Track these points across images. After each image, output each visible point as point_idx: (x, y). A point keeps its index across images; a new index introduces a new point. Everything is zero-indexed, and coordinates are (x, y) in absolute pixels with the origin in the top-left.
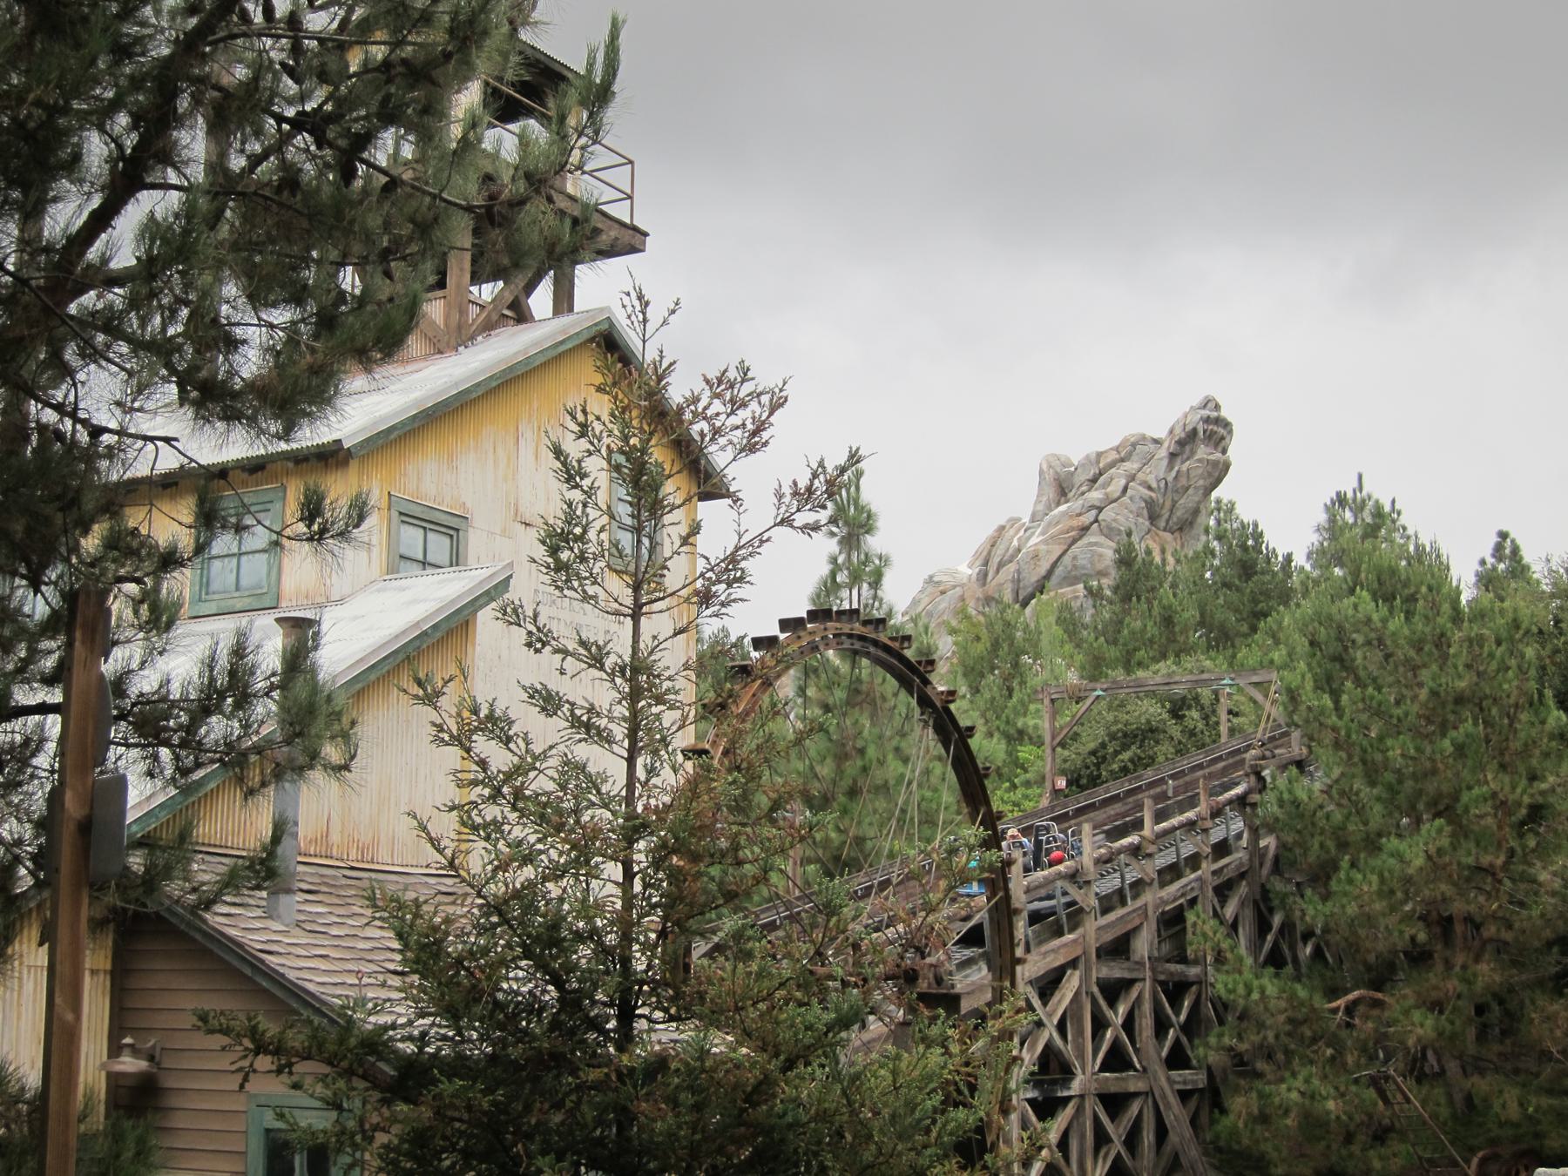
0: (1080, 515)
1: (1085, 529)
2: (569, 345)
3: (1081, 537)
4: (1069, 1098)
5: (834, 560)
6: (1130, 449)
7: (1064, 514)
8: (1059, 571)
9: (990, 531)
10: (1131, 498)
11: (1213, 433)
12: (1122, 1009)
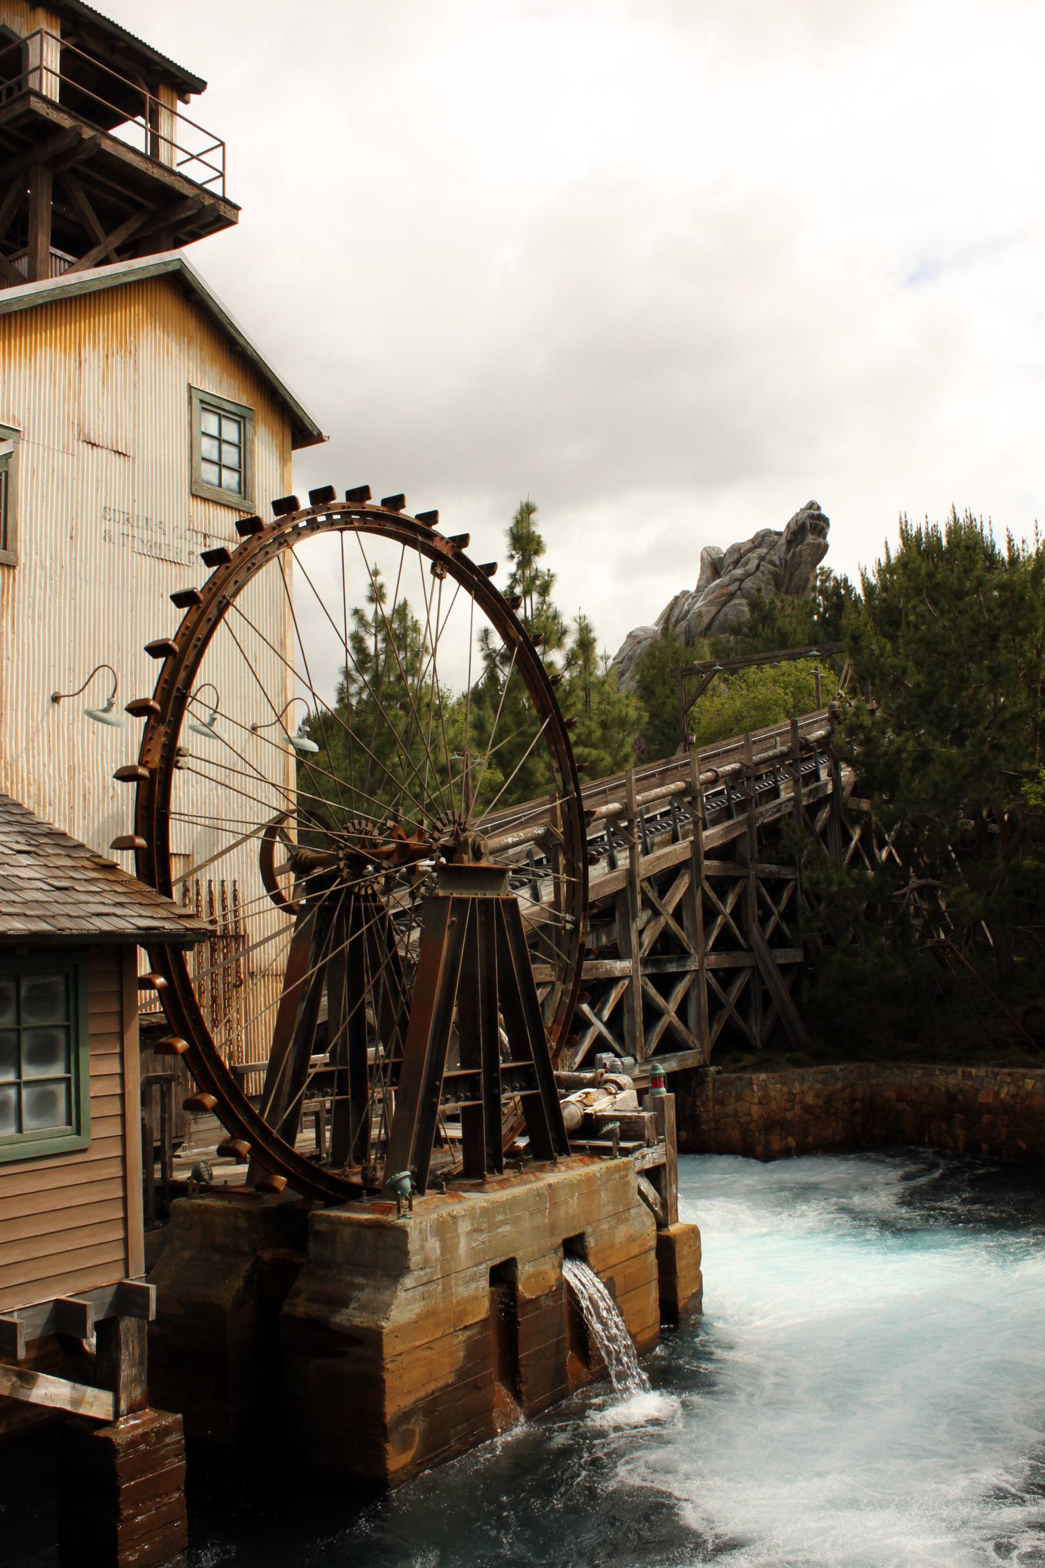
0: (728, 585)
1: (731, 596)
2: (132, 278)
3: (729, 600)
6: (763, 539)
7: (717, 585)
9: (669, 599)
10: (762, 573)
11: (816, 525)
12: (731, 900)
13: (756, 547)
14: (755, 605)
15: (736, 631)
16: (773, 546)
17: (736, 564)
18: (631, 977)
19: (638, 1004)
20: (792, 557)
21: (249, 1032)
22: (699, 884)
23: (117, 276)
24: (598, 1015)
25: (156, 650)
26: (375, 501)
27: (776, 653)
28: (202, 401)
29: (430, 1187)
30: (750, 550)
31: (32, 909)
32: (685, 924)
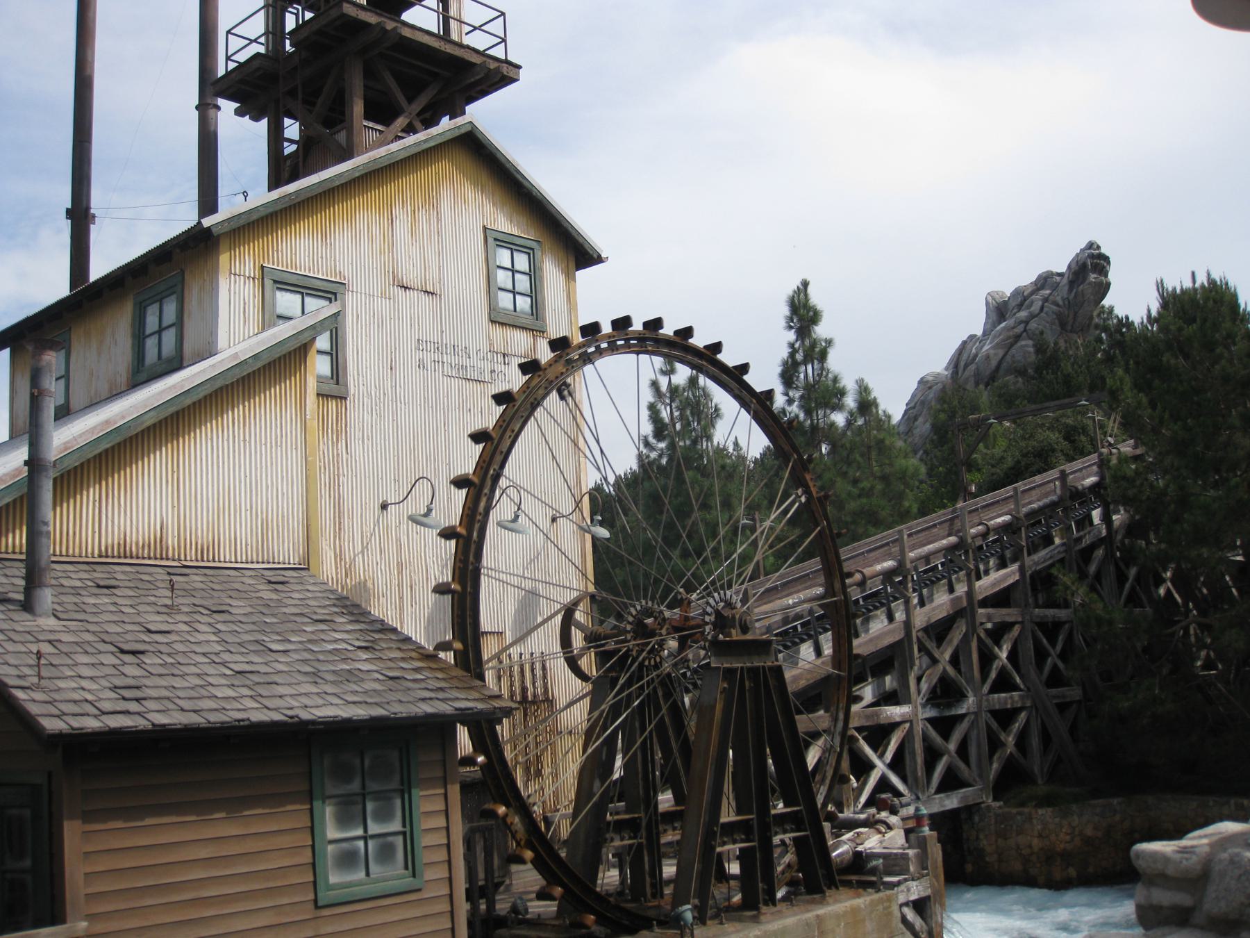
1: (1018, 338)
2: (432, 144)
3: (1016, 342)
4: (963, 716)
5: (792, 345)
6: (1045, 280)
8: (1004, 365)
9: (956, 345)
11: (1097, 264)
13: (1038, 289)
14: (1040, 349)
15: (1021, 372)
16: (1055, 287)
17: (1020, 306)
18: (911, 722)
19: (918, 746)
20: (1075, 297)
21: (555, 787)
22: (974, 630)
23: (418, 144)
24: (881, 756)
25: (477, 437)
26: (637, 326)
27: (1047, 404)
28: (495, 239)
29: (712, 918)
30: (1032, 293)
31: (371, 697)
32: (963, 670)
